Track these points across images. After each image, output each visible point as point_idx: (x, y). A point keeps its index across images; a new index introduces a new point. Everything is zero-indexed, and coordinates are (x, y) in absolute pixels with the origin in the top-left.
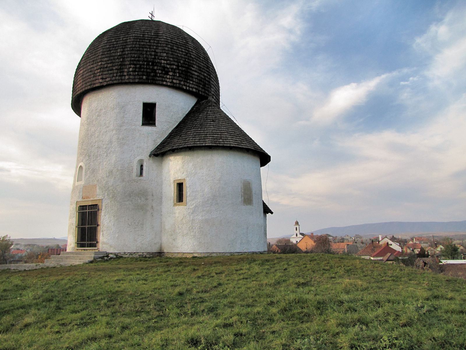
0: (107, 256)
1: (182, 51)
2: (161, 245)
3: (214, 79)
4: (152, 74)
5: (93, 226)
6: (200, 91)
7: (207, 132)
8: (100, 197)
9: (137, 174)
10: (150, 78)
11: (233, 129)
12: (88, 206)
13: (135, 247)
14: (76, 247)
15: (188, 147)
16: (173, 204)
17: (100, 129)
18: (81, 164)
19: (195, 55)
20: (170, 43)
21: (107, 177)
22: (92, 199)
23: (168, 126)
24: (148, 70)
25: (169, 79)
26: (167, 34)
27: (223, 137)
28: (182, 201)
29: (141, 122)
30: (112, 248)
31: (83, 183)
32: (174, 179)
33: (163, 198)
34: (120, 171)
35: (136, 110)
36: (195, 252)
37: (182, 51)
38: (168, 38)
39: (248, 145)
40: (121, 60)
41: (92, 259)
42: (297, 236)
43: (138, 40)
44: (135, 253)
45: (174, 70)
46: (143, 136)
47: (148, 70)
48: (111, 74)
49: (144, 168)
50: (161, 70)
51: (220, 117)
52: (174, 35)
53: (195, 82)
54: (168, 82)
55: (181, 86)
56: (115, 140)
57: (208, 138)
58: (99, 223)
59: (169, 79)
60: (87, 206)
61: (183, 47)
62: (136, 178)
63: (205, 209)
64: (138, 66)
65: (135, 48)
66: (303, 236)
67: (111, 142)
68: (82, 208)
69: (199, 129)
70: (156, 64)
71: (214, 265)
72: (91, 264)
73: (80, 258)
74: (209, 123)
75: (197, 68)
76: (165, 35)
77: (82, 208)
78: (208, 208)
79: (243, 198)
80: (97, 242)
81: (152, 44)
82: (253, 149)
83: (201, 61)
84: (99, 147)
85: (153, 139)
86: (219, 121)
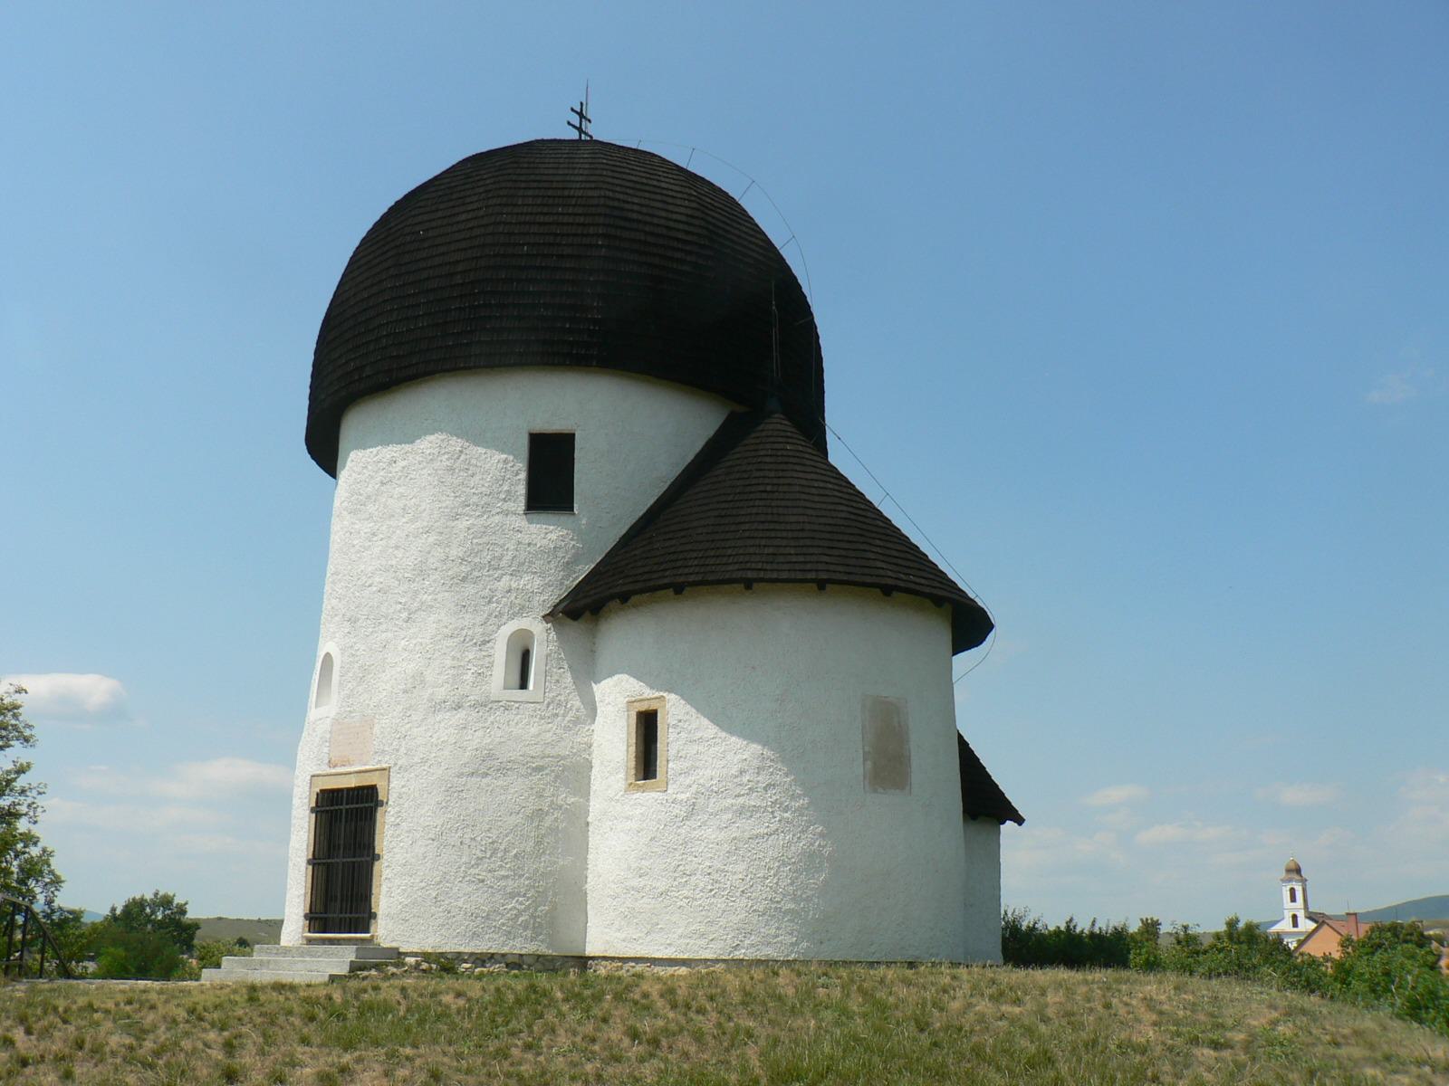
0: (399, 964)
14: (307, 929)
28: (654, 777)
31: (333, 714)
39: (884, 565)
42: (1295, 924)
66: (1316, 921)
78: (741, 800)
79: (869, 764)
80: (373, 916)
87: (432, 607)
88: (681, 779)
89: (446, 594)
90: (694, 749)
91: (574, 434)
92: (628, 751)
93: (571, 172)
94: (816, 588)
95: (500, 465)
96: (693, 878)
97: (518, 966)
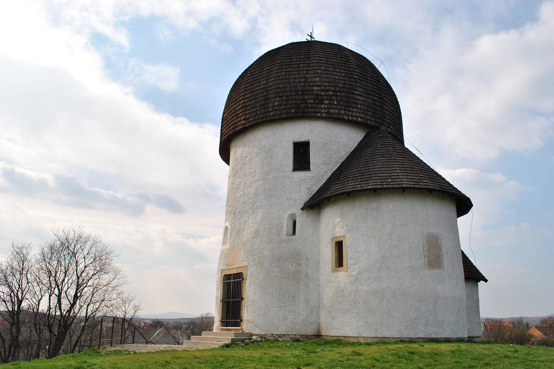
1: (340, 72)
2: (319, 325)
3: (390, 102)
4: (302, 106)
6: (368, 120)
8: (245, 263)
9: (287, 233)
11: (410, 164)
12: (232, 275)
13: (285, 328)
14: (221, 325)
15: (344, 193)
16: (331, 270)
17: (245, 180)
19: (359, 75)
20: (324, 65)
22: (236, 266)
23: (326, 169)
24: (298, 102)
25: (325, 108)
27: (394, 176)
29: (291, 168)
30: (257, 328)
33: (321, 262)
35: (285, 153)
36: (360, 336)
37: (340, 72)
38: (321, 59)
41: (228, 342)
43: (285, 67)
44: (285, 335)
45: (331, 97)
46: (294, 184)
47: (298, 102)
49: (297, 224)
51: (394, 151)
53: (361, 109)
54: (324, 113)
55: (341, 116)
57: (373, 178)
58: (243, 296)
59: (325, 108)
60: (231, 275)
61: (342, 68)
62: (287, 238)
67: (256, 194)
68: (227, 277)
69: (363, 169)
72: (228, 350)
74: (376, 159)
75: (363, 90)
76: (318, 56)
77: (227, 277)
78: (376, 274)
79: (426, 259)
80: (242, 320)
81: (302, 69)
82: (438, 189)
84: (244, 203)
85: (307, 187)
86: (391, 156)
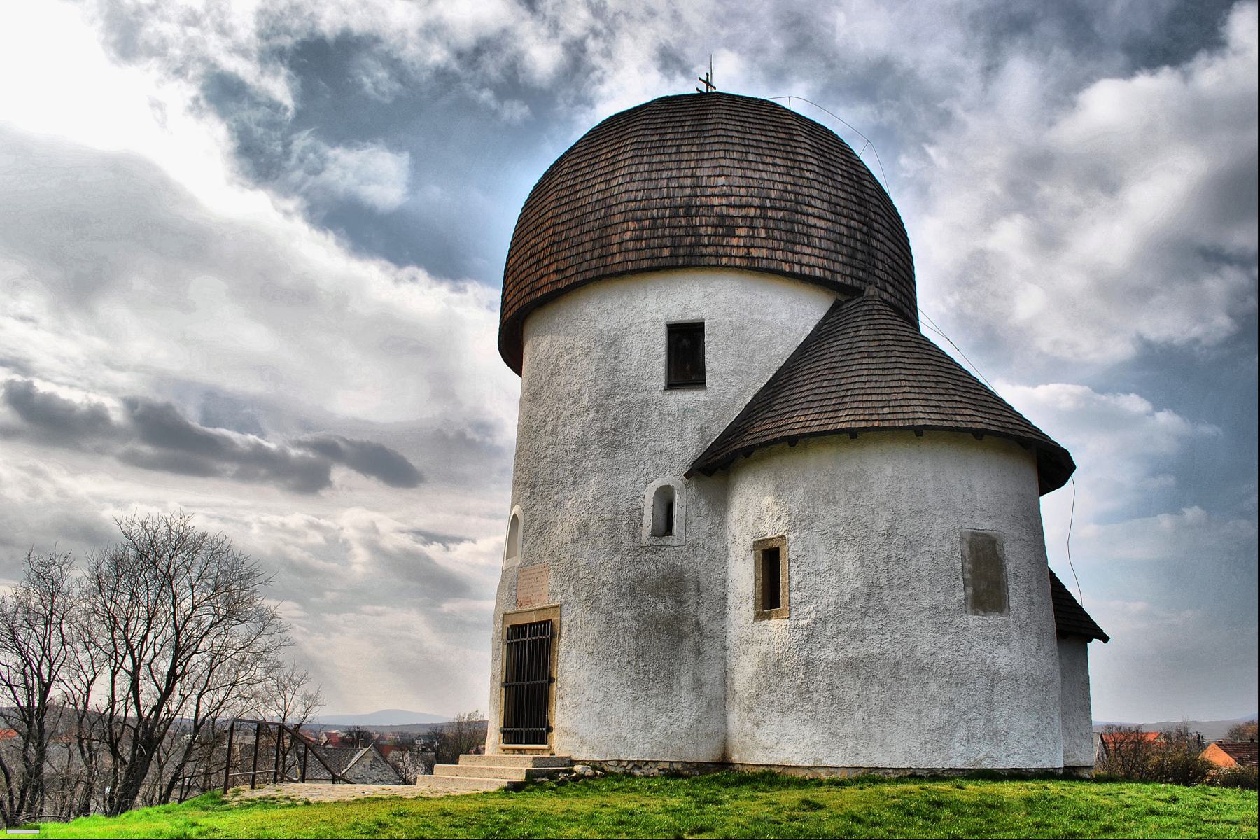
5: (539, 682)
6: (837, 272)
7: (848, 390)
10: (682, 251)
14: (502, 741)
16: (752, 614)
17: (558, 409)
18: (516, 509)
21: (573, 542)
22: (537, 605)
24: (677, 232)
26: (730, 122)
29: (662, 382)
32: (755, 540)
33: (730, 596)
34: (607, 523)
35: (648, 348)
36: (818, 764)
40: (603, 214)
44: (647, 762)
46: (669, 418)
47: (677, 232)
48: (578, 254)
50: (713, 226)
51: (896, 343)
52: (749, 123)
56: (593, 438)
60: (526, 625)
63: (845, 626)
64: (647, 222)
65: (638, 175)
67: (583, 443)
69: (825, 384)
70: (697, 211)
71: (385, 797)
73: (495, 775)
75: (825, 206)
78: (855, 625)
79: (970, 590)
80: (550, 730)
83: (839, 186)
87: (592, 471)
88: (801, 608)
89: (604, 460)
90: (810, 581)
91: (703, 323)
92: (756, 584)
93: (705, 117)
94: (914, 435)
95: (644, 352)
96: (815, 695)
97: (676, 775)
